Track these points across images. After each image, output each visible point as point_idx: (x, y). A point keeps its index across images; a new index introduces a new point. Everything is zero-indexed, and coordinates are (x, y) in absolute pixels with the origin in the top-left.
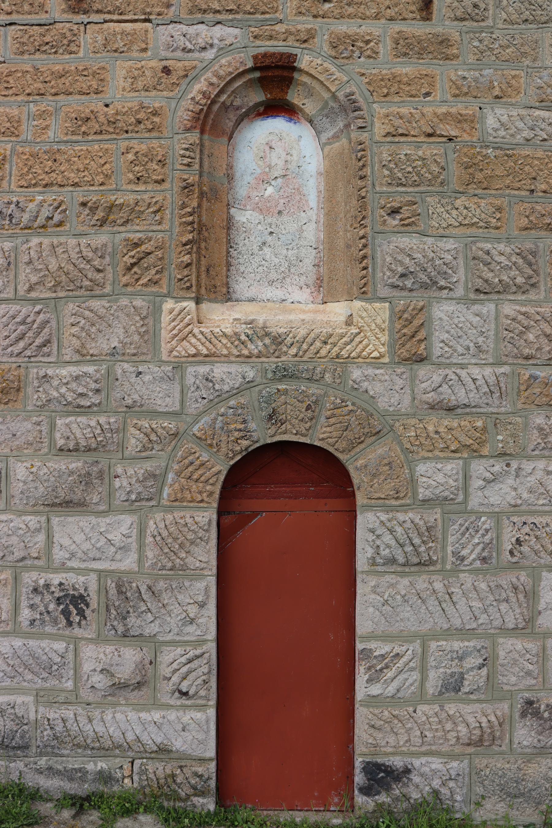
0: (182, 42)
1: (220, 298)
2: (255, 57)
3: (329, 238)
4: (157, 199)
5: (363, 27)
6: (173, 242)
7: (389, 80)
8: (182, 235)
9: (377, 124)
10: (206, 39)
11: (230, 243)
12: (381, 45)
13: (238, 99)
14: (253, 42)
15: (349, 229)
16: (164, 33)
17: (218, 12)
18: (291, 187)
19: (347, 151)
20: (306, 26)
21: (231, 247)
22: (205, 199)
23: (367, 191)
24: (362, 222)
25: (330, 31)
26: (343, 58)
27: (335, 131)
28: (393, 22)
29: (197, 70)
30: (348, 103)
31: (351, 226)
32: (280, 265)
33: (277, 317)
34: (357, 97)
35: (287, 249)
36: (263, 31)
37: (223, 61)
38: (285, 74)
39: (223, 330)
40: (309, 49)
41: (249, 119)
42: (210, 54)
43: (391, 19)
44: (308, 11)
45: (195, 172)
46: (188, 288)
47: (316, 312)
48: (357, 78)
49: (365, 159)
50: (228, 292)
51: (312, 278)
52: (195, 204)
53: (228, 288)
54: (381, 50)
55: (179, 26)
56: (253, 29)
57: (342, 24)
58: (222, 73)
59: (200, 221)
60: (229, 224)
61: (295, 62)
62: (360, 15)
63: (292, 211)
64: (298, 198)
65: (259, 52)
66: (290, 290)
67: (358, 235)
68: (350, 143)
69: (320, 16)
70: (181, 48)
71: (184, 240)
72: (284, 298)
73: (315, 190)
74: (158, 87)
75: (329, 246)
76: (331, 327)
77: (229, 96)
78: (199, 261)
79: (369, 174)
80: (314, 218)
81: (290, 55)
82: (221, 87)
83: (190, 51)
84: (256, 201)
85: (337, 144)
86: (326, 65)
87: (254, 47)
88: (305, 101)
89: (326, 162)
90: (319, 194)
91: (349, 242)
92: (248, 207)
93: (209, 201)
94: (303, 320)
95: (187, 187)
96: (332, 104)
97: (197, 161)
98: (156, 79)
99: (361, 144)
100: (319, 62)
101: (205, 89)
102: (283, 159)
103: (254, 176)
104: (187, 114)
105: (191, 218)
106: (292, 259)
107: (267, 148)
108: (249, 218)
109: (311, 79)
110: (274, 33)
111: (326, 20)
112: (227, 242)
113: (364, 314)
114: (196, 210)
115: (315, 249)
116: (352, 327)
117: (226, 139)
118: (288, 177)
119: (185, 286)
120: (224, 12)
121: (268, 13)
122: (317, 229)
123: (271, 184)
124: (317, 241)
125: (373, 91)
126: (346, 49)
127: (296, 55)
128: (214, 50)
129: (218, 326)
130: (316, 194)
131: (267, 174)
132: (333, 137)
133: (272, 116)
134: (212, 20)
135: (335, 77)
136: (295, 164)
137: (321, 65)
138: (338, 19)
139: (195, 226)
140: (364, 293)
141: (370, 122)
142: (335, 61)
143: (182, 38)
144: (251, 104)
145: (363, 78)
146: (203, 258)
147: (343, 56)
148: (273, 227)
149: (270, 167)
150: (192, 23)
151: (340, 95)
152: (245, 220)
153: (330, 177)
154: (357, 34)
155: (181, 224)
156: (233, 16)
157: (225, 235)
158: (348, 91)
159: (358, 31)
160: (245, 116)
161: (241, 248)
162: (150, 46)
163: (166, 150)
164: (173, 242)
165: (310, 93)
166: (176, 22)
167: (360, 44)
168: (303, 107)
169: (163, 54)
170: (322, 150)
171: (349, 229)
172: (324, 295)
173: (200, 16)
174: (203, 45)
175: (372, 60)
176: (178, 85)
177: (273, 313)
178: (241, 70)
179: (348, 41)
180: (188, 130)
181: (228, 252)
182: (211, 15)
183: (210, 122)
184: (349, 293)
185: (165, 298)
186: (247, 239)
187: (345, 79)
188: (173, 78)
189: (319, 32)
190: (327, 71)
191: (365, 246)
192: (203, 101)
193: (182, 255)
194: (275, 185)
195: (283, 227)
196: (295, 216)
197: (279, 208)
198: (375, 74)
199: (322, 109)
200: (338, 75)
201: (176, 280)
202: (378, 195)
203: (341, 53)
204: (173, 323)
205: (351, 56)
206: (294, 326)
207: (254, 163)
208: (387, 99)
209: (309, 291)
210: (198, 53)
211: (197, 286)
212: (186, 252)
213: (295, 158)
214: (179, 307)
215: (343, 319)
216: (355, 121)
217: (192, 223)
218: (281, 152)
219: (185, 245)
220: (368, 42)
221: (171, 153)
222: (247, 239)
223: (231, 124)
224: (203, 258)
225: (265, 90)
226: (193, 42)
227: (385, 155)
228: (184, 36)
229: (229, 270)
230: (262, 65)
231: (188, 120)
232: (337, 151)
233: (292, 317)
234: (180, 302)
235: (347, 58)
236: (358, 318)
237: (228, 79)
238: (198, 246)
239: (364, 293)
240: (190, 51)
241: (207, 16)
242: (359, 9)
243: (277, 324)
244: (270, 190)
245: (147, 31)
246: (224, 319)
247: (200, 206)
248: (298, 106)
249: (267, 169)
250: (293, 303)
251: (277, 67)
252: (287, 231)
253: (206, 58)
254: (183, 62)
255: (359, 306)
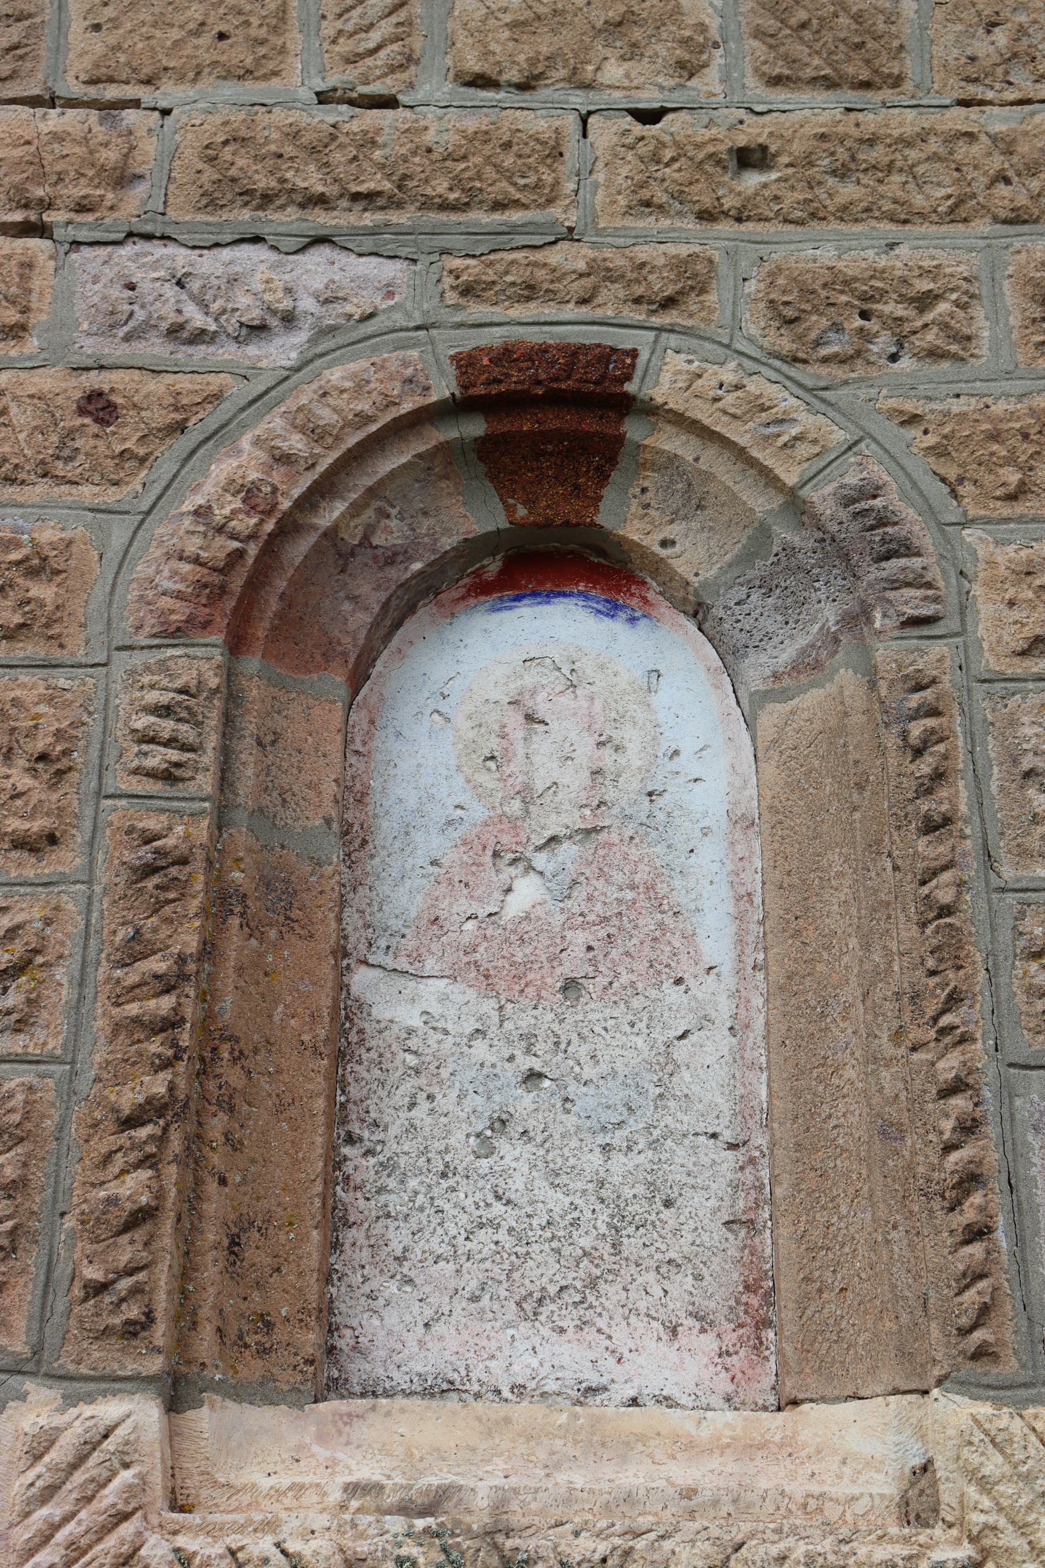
0: (171, 305)
1: (287, 1379)
2: (465, 363)
3: (797, 1094)
4: (19, 918)
5: (903, 250)
6: (79, 1110)
7: (1026, 436)
8: (119, 1081)
9: (986, 608)
10: (267, 297)
11: (345, 1121)
12: (979, 312)
13: (393, 523)
14: (457, 307)
15: (889, 1050)
16: (95, 277)
17: (321, 201)
18: (618, 877)
19: (857, 719)
20: (672, 249)
21: (351, 1139)
22: (235, 921)
23: (960, 884)
24: (945, 1020)
25: (767, 267)
26: (825, 360)
27: (802, 641)
28: (1026, 228)
29: (226, 409)
30: (855, 526)
31: (897, 1036)
32: (575, 1223)
33: (561, 1477)
34: (891, 500)
35: (606, 1148)
36: (500, 268)
37: (335, 376)
38: (590, 424)
39: (292, 1547)
40: (686, 332)
41: (440, 605)
42: (281, 351)
43: (1016, 219)
44: (679, 196)
45: (197, 806)
46: (133, 1330)
47: (752, 1448)
48: (890, 432)
49: (941, 748)
50: (331, 1350)
51: (722, 1281)
52: (188, 939)
53: (332, 1329)
54: (981, 323)
55: (159, 250)
56: (457, 263)
57: (817, 243)
58: (326, 416)
59: (209, 1016)
60: (343, 1037)
61: (628, 378)
62: (887, 206)
63: (625, 978)
64: (648, 923)
65: (482, 343)
66: (621, 1337)
67: (932, 1076)
68: (873, 685)
69: (726, 214)
70: (164, 326)
71: (128, 1099)
72: (595, 1381)
73: (725, 891)
74: (60, 468)
75: (796, 1134)
76: (829, 1528)
77: (355, 509)
78: (192, 1198)
79: (963, 808)
80: (724, 1009)
81: (607, 355)
82: (321, 468)
83: (200, 337)
84: (466, 939)
85: (815, 695)
86: (753, 386)
87: (460, 325)
88: (668, 532)
89: (770, 770)
90: (744, 905)
91: (892, 1112)
92: (431, 965)
93: (252, 928)
94: (689, 1493)
95: (156, 870)
96: (785, 534)
97: (208, 758)
98: (54, 438)
99: (919, 688)
100: (728, 376)
101: (253, 475)
102: (580, 762)
103: (455, 834)
104: (174, 573)
105: (165, 1004)
106: (628, 1192)
107: (515, 720)
108: (435, 1009)
109: (694, 441)
110: (541, 274)
111: (750, 226)
112: (329, 1114)
113: (993, 1465)
114: (191, 967)
115: (733, 1146)
116: (938, 1531)
117: (337, 680)
118: (603, 837)
119: (117, 1321)
120: (344, 203)
121: (517, 204)
122: (738, 1057)
123: (530, 868)
124: (743, 1103)
125: (961, 480)
126: (837, 327)
127: (634, 354)
128: (300, 337)
129: (269, 1526)
130: (729, 907)
131: (514, 823)
132: (796, 667)
133: (534, 594)
134: (294, 228)
135: (794, 432)
136: (636, 785)
137: (738, 387)
138: (799, 222)
139: (185, 1039)
140: (981, 1353)
141: (953, 600)
142: (792, 372)
143: (170, 291)
144: (447, 543)
145: (914, 432)
146: (212, 1187)
147: (824, 351)
148: (540, 1048)
149: (526, 795)
150: (214, 238)
151: (822, 497)
152: (416, 1022)
153: (789, 829)
154: (877, 273)
155: (117, 1028)
156: (379, 217)
157: (320, 1083)
158: (852, 479)
159: (883, 262)
160: (424, 593)
161: (395, 1143)
162: (38, 319)
163: (75, 713)
164: (79, 1110)
165: (694, 499)
166: (148, 237)
167: (890, 308)
168: (663, 553)
169: (90, 347)
170: (750, 725)
171: (889, 1050)
172: (783, 1363)
173: (246, 215)
174: (254, 315)
175: (945, 365)
176: (143, 460)
177: (542, 1454)
178: (407, 407)
179: (844, 298)
180: (173, 633)
181: (335, 1163)
182: (292, 213)
183: (274, 605)
184: (905, 1355)
185: (14, 1381)
186: (424, 1106)
187: (839, 436)
188: (126, 436)
189: (723, 269)
190: (763, 409)
191: (969, 1127)
192: (246, 523)
193: (115, 1168)
194: (549, 869)
195: (583, 1051)
196: (636, 1003)
197: (567, 968)
198: (963, 415)
199: (746, 558)
200: (806, 421)
201: (77, 1292)
202: (1010, 898)
203: (818, 343)
204: (44, 1512)
205: (858, 353)
206: (644, 1521)
207: (460, 780)
208: (1019, 508)
209: (708, 1343)
210: (233, 347)
211: (177, 1318)
212: (134, 1156)
213: (634, 757)
214: (78, 1428)
215: (885, 1485)
216: (891, 595)
217: (170, 1024)
218: (573, 736)
219: (130, 1122)
220: (924, 301)
221: (95, 728)
222: (424, 1106)
223: (360, 620)
224: (212, 1187)
225: (505, 491)
226: (215, 307)
227: (1029, 731)
228: (180, 284)
229: (336, 1246)
230: (494, 389)
231: (179, 596)
232: (817, 725)
233: (633, 1476)
234: (90, 1398)
235: (843, 360)
236: (962, 1481)
237: (353, 439)
238: (191, 1128)
239: (981, 1353)
240: (200, 337)
241: (275, 216)
242: (881, 189)
243: (557, 1513)
244: (527, 892)
245: (28, 265)
246: (298, 1489)
247: (209, 950)
248: (644, 552)
249: (515, 807)
250: (634, 1402)
251: (556, 399)
252: (604, 1068)
253: (263, 364)
254: (169, 379)
255: (966, 1423)
